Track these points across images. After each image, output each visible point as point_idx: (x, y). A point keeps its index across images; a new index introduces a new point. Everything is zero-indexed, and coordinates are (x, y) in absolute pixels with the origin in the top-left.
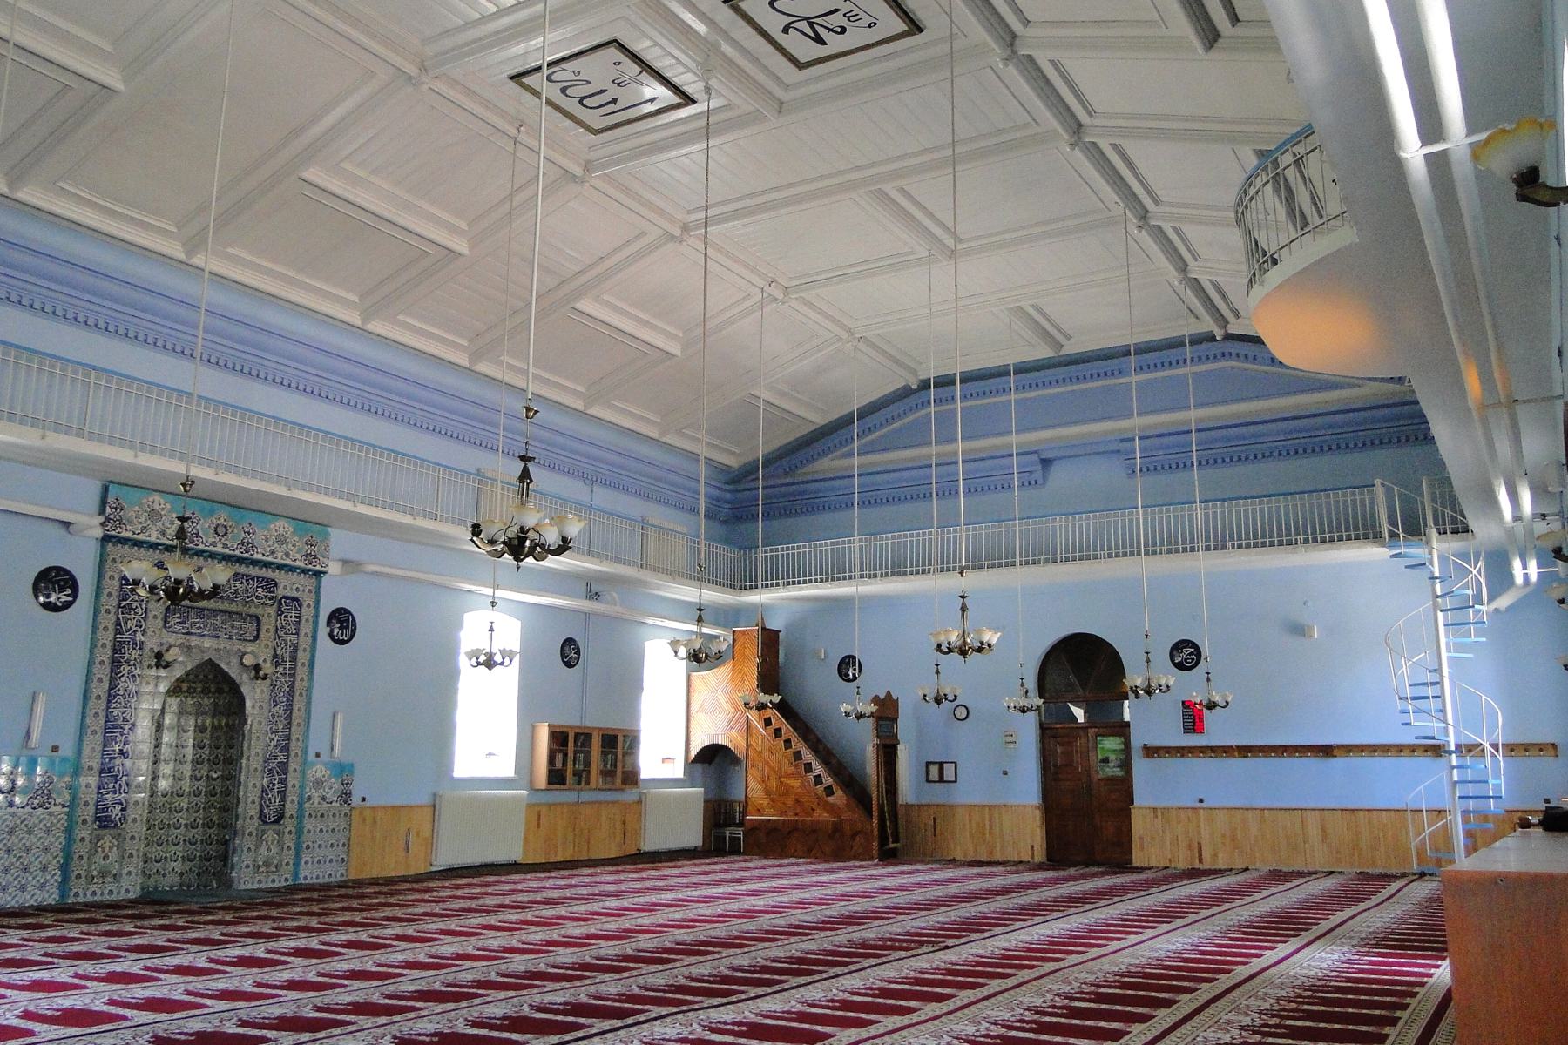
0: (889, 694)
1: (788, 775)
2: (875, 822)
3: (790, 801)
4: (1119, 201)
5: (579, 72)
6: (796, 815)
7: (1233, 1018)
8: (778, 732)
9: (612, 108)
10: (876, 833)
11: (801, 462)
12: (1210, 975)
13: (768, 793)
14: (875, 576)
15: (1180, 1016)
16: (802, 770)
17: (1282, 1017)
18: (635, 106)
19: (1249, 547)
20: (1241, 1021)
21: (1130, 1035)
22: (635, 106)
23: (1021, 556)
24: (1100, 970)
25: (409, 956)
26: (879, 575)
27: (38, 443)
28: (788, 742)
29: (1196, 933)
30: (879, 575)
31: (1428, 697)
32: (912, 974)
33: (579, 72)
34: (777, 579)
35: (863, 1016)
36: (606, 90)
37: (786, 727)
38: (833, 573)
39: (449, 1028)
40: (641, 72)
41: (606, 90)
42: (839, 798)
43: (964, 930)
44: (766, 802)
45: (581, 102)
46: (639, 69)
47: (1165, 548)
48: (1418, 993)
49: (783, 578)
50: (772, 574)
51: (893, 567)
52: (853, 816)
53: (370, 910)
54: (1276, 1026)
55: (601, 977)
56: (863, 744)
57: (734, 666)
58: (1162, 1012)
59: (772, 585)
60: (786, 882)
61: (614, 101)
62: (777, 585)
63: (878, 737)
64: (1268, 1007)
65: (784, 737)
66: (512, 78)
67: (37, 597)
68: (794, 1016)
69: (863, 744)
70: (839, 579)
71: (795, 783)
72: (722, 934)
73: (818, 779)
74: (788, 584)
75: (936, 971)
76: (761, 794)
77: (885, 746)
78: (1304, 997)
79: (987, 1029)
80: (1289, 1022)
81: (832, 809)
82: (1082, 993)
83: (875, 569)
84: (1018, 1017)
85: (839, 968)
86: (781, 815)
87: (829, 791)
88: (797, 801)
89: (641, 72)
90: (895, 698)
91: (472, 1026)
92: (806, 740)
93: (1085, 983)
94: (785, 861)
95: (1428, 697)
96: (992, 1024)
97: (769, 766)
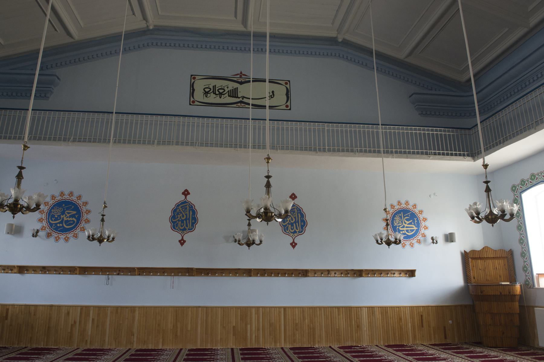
7: (166, 357)
15: (123, 357)
17: (211, 358)
19: (348, 152)
20: (164, 356)
21: (129, 355)
31: (252, 99)
32: (42, 357)
35: (33, 352)
36: (268, 225)
41: (268, 225)
48: (188, 351)
54: (159, 352)
58: (128, 357)
64: (112, 352)
67: (26, 150)
78: (156, 356)
79: (54, 352)
80: (156, 353)
84: (55, 351)
85: (23, 352)
95: (252, 99)
96: (101, 359)
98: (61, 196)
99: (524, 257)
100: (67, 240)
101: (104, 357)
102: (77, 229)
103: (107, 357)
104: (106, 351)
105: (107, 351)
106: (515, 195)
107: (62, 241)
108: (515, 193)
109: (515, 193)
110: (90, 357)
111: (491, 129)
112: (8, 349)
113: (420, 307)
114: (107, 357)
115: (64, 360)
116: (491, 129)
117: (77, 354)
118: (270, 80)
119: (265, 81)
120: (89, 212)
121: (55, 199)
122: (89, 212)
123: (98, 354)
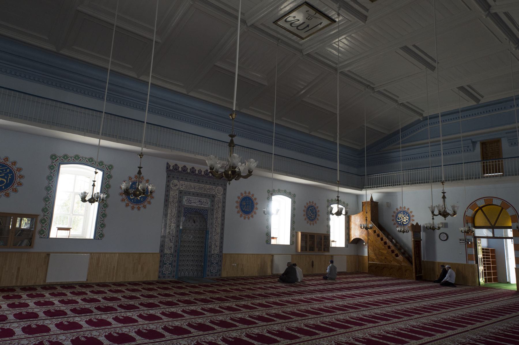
0: (417, 224)
1: (383, 249)
2: (414, 267)
3: (383, 258)
4: (507, 38)
5: (295, 17)
6: (386, 262)
8: (378, 236)
9: (307, 29)
10: (414, 271)
11: (423, 126)
12: (516, 311)
13: (375, 254)
14: (409, 184)
16: (387, 248)
18: (315, 26)
22: (315, 26)
23: (465, 176)
24: (480, 309)
25: (270, 285)
26: (410, 184)
27: (195, 157)
28: (382, 239)
29: (515, 300)
30: (410, 184)
33: (295, 17)
34: (386, 184)
37: (381, 233)
38: (393, 183)
39: (281, 329)
40: (316, 13)
42: (400, 257)
43: (438, 295)
44: (375, 258)
45: (297, 28)
46: (315, 12)
47: (474, 177)
49: (376, 185)
50: (370, 184)
51: (397, 183)
52: (405, 264)
53: (256, 279)
55: (320, 286)
56: (408, 239)
57: (363, 213)
59: (372, 187)
60: (389, 289)
61: (308, 26)
62: (374, 187)
63: (414, 238)
65: (380, 237)
66: (274, 23)
68: (396, 333)
69: (408, 239)
70: (395, 185)
71: (385, 252)
72: (355, 286)
73: (393, 252)
74: (378, 187)
75: (429, 306)
76: (373, 255)
77: (416, 241)
81: (398, 261)
82: (499, 333)
83: (409, 182)
86: (380, 262)
87: (397, 255)
88: (386, 258)
89: (316, 13)
90: (420, 225)
91: (287, 329)
92: (388, 238)
93: (499, 330)
94: (383, 278)
97: (376, 246)
98: (12, 163)
99: (294, 201)
100: (149, 203)
101: (477, 338)
102: (14, 184)
103: (473, 336)
104: (501, 333)
105: (500, 333)
106: (71, 158)
107: (148, 206)
108: (73, 158)
109: (73, 158)
110: (406, 333)
111: (493, 168)
112: (398, 328)
113: (254, 254)
114: (473, 336)
115: (423, 339)
116: (493, 168)
117: (442, 333)
118: (438, 145)
119: (105, 113)
120: (409, 209)
121: (13, 165)
122: (409, 209)
123: (502, 336)
